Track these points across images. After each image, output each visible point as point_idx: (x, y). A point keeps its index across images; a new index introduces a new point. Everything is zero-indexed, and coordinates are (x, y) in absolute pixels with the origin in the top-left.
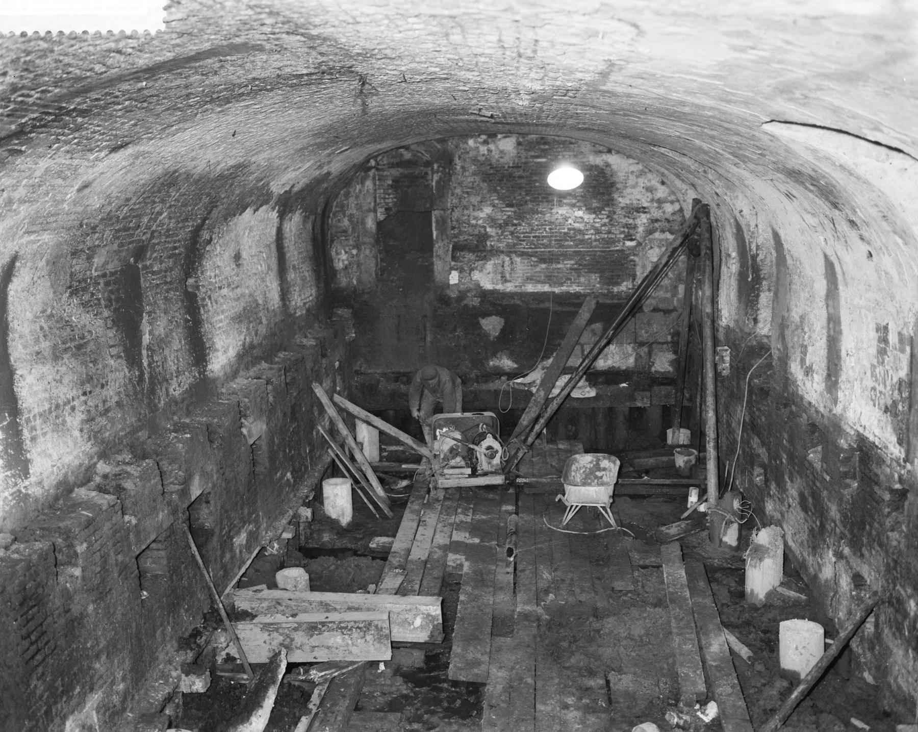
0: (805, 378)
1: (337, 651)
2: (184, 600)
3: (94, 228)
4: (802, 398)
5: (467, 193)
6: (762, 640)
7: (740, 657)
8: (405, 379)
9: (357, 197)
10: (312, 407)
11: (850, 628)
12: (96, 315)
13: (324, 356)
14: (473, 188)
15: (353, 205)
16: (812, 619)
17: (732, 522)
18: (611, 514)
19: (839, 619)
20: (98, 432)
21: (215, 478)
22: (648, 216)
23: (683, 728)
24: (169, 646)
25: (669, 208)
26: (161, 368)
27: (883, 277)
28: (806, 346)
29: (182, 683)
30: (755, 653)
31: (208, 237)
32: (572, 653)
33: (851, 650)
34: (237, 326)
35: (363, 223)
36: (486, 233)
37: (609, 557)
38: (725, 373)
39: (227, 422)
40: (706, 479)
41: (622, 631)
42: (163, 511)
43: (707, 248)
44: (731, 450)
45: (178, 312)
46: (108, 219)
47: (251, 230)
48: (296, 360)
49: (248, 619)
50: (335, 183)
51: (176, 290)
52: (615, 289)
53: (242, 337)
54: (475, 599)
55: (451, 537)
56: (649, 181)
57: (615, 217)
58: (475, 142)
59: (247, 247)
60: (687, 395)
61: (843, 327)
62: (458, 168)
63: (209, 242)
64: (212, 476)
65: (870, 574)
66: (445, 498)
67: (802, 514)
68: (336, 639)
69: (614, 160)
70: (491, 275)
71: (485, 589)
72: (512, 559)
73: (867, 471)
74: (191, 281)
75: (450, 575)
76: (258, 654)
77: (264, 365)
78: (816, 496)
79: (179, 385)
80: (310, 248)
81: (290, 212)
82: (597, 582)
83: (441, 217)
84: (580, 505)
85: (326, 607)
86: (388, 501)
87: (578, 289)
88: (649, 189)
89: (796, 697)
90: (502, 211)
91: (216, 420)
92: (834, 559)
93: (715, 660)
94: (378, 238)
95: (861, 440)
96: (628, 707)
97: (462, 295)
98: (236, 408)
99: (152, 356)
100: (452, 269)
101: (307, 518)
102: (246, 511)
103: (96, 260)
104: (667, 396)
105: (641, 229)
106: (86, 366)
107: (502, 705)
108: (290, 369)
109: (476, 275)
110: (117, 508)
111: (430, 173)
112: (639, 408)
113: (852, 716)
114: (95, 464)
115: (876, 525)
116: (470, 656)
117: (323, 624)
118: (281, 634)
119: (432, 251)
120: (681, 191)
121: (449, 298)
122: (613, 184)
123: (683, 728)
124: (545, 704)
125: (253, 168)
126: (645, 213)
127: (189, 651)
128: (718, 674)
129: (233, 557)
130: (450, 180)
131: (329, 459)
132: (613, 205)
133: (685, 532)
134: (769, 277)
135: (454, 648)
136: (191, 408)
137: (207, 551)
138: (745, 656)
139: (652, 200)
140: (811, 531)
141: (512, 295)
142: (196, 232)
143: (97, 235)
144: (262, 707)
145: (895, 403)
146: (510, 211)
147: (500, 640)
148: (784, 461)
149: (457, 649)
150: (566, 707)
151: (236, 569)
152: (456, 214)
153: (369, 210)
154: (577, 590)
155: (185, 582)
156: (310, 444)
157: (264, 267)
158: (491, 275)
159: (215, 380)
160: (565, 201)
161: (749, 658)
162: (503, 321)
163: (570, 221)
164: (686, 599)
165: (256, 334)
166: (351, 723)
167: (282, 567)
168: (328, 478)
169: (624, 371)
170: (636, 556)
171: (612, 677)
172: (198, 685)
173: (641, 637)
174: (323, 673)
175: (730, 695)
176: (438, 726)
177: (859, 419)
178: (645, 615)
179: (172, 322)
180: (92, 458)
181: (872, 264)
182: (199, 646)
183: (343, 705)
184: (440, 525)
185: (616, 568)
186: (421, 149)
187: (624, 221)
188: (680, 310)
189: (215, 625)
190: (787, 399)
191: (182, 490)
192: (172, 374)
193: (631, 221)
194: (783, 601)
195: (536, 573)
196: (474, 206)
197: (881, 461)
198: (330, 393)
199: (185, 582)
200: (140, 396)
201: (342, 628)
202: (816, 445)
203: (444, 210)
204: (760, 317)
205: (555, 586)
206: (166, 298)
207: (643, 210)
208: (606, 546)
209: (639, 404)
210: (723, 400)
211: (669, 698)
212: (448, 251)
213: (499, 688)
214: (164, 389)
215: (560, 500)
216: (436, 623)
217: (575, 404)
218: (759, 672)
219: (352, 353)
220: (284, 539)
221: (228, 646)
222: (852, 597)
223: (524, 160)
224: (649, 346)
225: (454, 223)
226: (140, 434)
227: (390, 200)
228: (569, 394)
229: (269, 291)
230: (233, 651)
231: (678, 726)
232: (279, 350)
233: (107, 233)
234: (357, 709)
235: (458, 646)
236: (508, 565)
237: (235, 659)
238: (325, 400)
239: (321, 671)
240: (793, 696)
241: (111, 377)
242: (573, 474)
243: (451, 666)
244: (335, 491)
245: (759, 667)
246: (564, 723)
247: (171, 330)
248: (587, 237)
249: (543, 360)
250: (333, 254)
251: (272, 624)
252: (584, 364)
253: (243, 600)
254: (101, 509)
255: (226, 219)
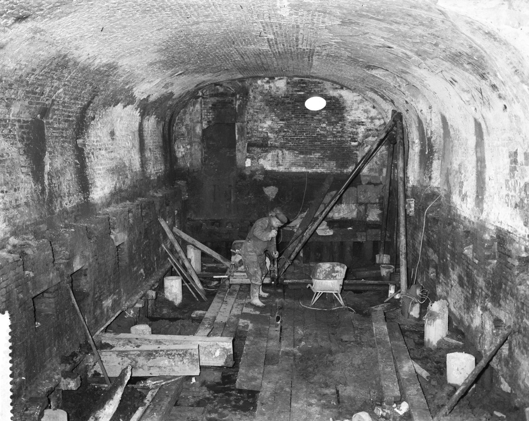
0: (462, 202)
1: (165, 370)
2: (67, 333)
3: (11, 85)
4: (460, 216)
5: (257, 112)
6: (435, 367)
7: (422, 377)
8: (218, 224)
9: (191, 114)
10: (159, 233)
11: (493, 349)
12: (13, 144)
13: (168, 205)
14: (260, 109)
15: (188, 119)
16: (467, 352)
17: (416, 303)
18: (341, 300)
19: (485, 350)
20: (11, 218)
21: (91, 261)
22: (365, 127)
23: (386, 418)
24: (54, 360)
25: (378, 123)
26: (57, 188)
27: (514, 120)
28: (463, 182)
29: (61, 384)
30: (431, 375)
31: (92, 115)
32: (315, 374)
33: (492, 368)
34: (111, 175)
35: (194, 130)
36: (268, 136)
37: (340, 322)
38: (412, 214)
39: (100, 228)
40: (400, 281)
41: (347, 361)
42: (53, 273)
43: (401, 138)
44: (415, 261)
45: (70, 157)
46: (20, 81)
47: (121, 118)
48: (149, 202)
49: (109, 348)
50: (177, 103)
51: (70, 143)
52: (345, 171)
53: (114, 183)
54: (256, 343)
55: (242, 310)
56: (366, 106)
57: (345, 127)
58: (262, 82)
59: (119, 129)
60: (388, 235)
61: (487, 163)
62: (251, 97)
63: (93, 118)
64: (89, 259)
65: (505, 316)
66: (240, 290)
67: (460, 289)
68: (165, 362)
69: (345, 93)
70: (271, 162)
71: (262, 339)
72: (279, 322)
73: (503, 250)
74: (80, 141)
75: (241, 332)
76: (114, 372)
77: (128, 202)
78: (469, 275)
79: (70, 202)
80: (161, 140)
81: (148, 115)
82: (332, 336)
83: (241, 126)
84: (322, 292)
85: (159, 342)
86: (204, 292)
87: (322, 170)
88: (366, 111)
89: (459, 394)
90: (278, 124)
91: (93, 225)
92: (481, 312)
93: (406, 376)
94: (203, 139)
95: (499, 231)
96: (351, 406)
97: (253, 173)
98: (107, 221)
99: (51, 180)
100: (247, 157)
101: (152, 297)
102: (112, 286)
103: (13, 108)
104: (376, 235)
105: (361, 135)
106: (4, 175)
107: (270, 403)
108: (145, 207)
109: (262, 162)
110: (19, 263)
111: (234, 100)
112: (359, 243)
113: (494, 410)
114: (8, 238)
115: (509, 283)
116: (250, 375)
117: (156, 352)
118: (129, 359)
119: (235, 148)
120: (384, 110)
121: (245, 175)
122: (344, 108)
123: (386, 418)
124: (297, 403)
125: (120, 71)
126: (363, 125)
127: (68, 365)
128: (408, 383)
129: (102, 313)
130: (246, 104)
131: (169, 266)
132: (344, 120)
133: (387, 310)
134: (439, 151)
135: (240, 370)
136: (78, 218)
137: (84, 305)
138: (425, 377)
139: (367, 118)
140: (466, 298)
141: (283, 174)
142: (85, 109)
143: (13, 91)
144: (112, 399)
145: (522, 200)
146: (282, 123)
147: (270, 367)
148: (448, 259)
149: (242, 370)
150: (311, 405)
151: (104, 321)
152: (250, 125)
153: (198, 122)
154: (319, 340)
155: (67, 321)
156: (157, 255)
157: (130, 145)
158: (271, 162)
159: (94, 205)
160: (315, 118)
161: (427, 377)
162: (277, 189)
163: (318, 130)
164: (387, 342)
165: (124, 183)
166: (172, 413)
167: (136, 324)
168: (168, 276)
169: (350, 220)
170: (356, 323)
171: (340, 388)
172: (72, 385)
173: (359, 365)
174: (155, 382)
175: (416, 395)
176: (228, 415)
177: (498, 218)
178: (361, 352)
179: (66, 162)
180: (6, 233)
181: (506, 114)
182: (75, 362)
183: (166, 402)
184: (236, 304)
185: (343, 328)
186: (229, 86)
187: (350, 130)
188: (384, 184)
189: (86, 351)
190: (451, 219)
191: (68, 263)
192: (65, 194)
193: (355, 130)
194: (449, 346)
195: (294, 330)
196: (261, 120)
197: (512, 241)
198: (171, 228)
199: (67, 321)
200: (42, 202)
201: (168, 355)
202: (468, 245)
203: (243, 122)
204: (433, 176)
205: (306, 337)
206: (62, 146)
207: (362, 123)
208: (338, 316)
209: (359, 240)
210: (410, 232)
211: (376, 401)
212: (245, 147)
213: (268, 394)
214: (59, 202)
215: (309, 287)
216: (229, 354)
217: (320, 239)
218: (434, 386)
219: (185, 208)
220: (137, 308)
221: (95, 365)
222: (493, 334)
223: (291, 93)
224: (366, 205)
225: (249, 130)
226: (41, 226)
227: (211, 116)
228: (315, 231)
229: (133, 160)
230: (99, 369)
231: (382, 416)
232: (138, 197)
233: (20, 91)
234: (176, 405)
235: (243, 369)
236: (277, 326)
237: (100, 374)
238: (167, 229)
239: (153, 381)
240: (457, 393)
241: (21, 185)
242: (318, 274)
243: (238, 380)
244: (172, 283)
245: (434, 383)
246: (309, 414)
247: (65, 167)
248: (328, 139)
249: (301, 213)
250: (176, 148)
251: (124, 352)
252: (326, 210)
253: (107, 338)
254: (8, 262)
255: (104, 107)
